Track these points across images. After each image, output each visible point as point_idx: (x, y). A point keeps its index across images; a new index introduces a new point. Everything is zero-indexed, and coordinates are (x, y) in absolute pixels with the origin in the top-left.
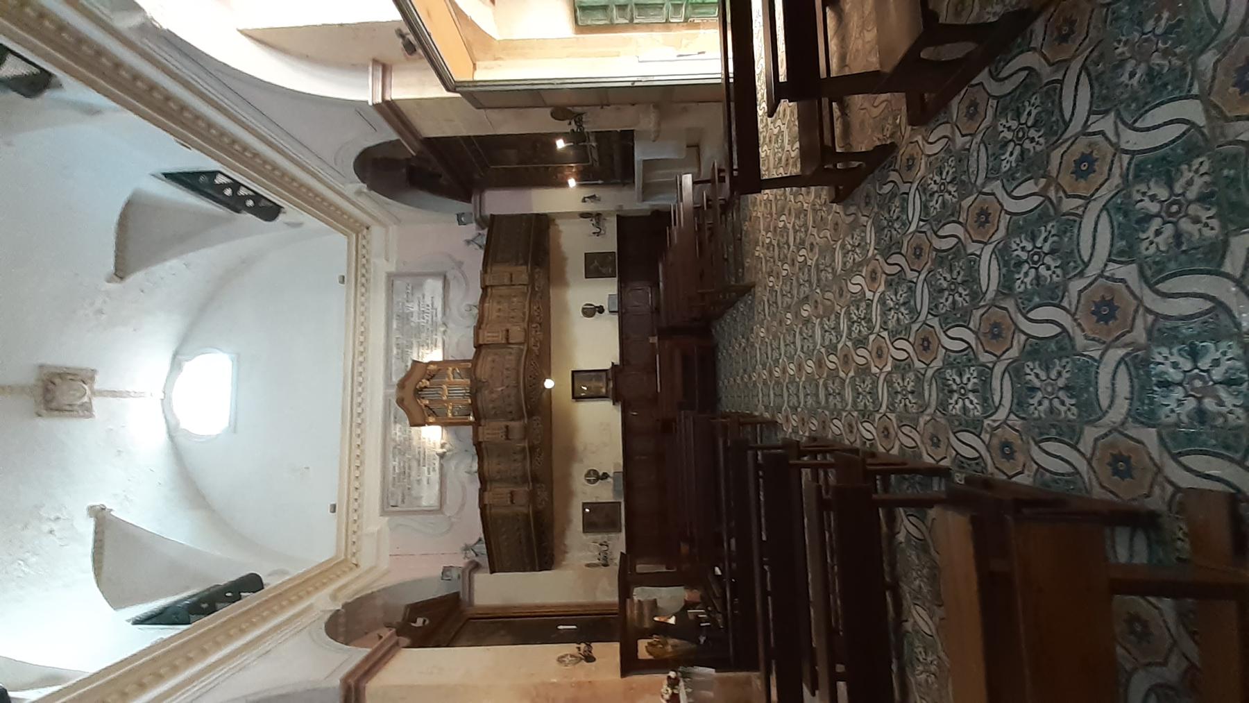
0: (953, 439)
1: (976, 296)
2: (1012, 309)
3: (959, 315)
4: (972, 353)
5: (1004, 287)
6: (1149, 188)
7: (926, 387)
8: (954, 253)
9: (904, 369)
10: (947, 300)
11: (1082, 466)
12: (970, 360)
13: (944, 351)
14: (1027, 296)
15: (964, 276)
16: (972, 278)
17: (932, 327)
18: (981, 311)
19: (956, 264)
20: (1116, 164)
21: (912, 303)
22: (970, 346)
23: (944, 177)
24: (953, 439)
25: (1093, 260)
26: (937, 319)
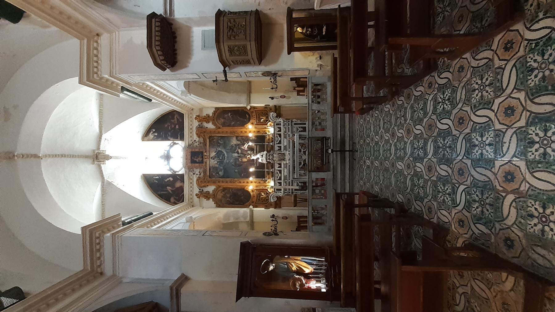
0: (438, 168)
1: (435, 141)
2: (425, 134)
3: (442, 134)
4: (438, 118)
5: (426, 142)
6: (534, 56)
7: (463, 97)
8: (442, 162)
9: (480, 104)
10: (440, 107)
11: (492, 177)
12: (439, 115)
13: (451, 118)
14: (421, 137)
15: (439, 150)
16: (437, 148)
17: (456, 130)
18: (433, 135)
19: (441, 156)
20: (522, 44)
21: (468, 145)
22: (439, 121)
23: (442, 106)
24: (438, 168)
25: (508, 88)
26: (453, 134)
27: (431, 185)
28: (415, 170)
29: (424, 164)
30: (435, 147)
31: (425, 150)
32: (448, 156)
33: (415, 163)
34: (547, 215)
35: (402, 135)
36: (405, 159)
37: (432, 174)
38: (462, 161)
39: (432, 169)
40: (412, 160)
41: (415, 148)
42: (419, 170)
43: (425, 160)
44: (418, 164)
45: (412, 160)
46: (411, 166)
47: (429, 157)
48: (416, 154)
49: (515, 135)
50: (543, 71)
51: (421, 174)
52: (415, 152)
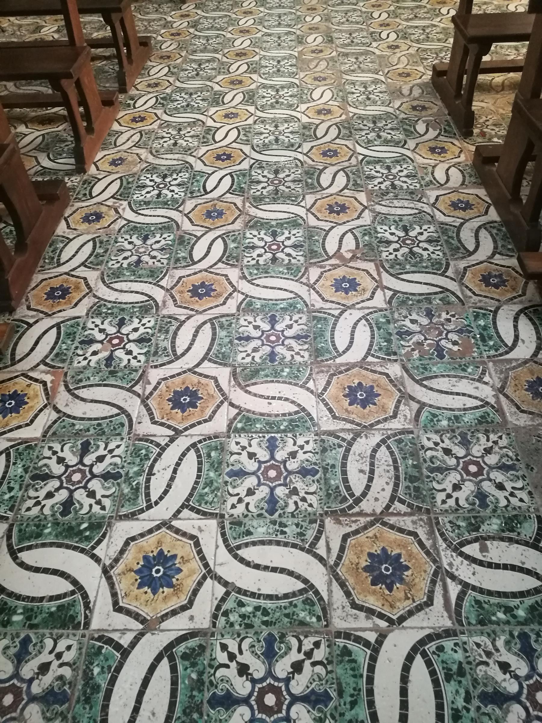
1: (258, 200)
2: (230, 228)
21: (274, 147)
27: (383, 203)
28: (354, 258)
29: (326, 226)
30: (274, 201)
31: (282, 224)
32: (244, 355)
33: (330, 258)
34: (23, 709)
35: (341, 173)
36: (319, 304)
37: (351, 202)
38: (222, 402)
39: (336, 203)
40: (319, 271)
41: (274, 259)
42: (349, 243)
43: (312, 221)
44: (331, 246)
45: (319, 271)
46: (340, 273)
47: (301, 212)
48: (294, 254)
49: (300, 585)
50: (523, 698)
51: (365, 235)
52: (287, 259)
